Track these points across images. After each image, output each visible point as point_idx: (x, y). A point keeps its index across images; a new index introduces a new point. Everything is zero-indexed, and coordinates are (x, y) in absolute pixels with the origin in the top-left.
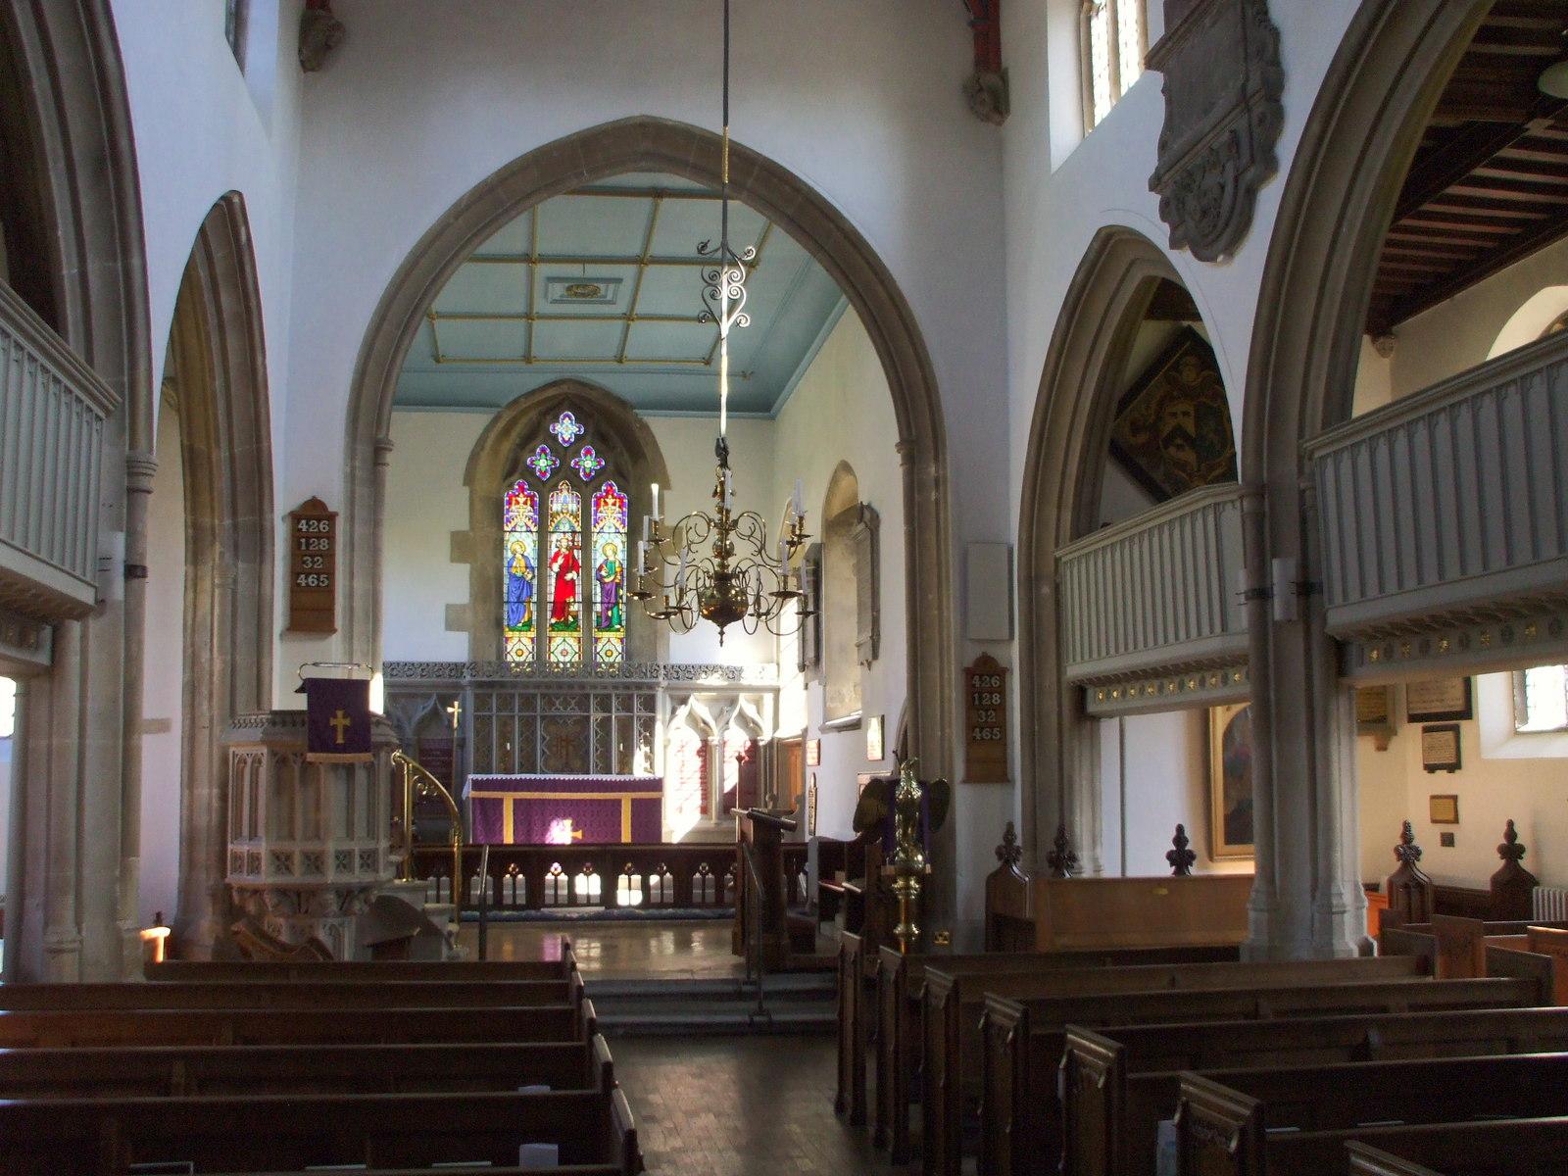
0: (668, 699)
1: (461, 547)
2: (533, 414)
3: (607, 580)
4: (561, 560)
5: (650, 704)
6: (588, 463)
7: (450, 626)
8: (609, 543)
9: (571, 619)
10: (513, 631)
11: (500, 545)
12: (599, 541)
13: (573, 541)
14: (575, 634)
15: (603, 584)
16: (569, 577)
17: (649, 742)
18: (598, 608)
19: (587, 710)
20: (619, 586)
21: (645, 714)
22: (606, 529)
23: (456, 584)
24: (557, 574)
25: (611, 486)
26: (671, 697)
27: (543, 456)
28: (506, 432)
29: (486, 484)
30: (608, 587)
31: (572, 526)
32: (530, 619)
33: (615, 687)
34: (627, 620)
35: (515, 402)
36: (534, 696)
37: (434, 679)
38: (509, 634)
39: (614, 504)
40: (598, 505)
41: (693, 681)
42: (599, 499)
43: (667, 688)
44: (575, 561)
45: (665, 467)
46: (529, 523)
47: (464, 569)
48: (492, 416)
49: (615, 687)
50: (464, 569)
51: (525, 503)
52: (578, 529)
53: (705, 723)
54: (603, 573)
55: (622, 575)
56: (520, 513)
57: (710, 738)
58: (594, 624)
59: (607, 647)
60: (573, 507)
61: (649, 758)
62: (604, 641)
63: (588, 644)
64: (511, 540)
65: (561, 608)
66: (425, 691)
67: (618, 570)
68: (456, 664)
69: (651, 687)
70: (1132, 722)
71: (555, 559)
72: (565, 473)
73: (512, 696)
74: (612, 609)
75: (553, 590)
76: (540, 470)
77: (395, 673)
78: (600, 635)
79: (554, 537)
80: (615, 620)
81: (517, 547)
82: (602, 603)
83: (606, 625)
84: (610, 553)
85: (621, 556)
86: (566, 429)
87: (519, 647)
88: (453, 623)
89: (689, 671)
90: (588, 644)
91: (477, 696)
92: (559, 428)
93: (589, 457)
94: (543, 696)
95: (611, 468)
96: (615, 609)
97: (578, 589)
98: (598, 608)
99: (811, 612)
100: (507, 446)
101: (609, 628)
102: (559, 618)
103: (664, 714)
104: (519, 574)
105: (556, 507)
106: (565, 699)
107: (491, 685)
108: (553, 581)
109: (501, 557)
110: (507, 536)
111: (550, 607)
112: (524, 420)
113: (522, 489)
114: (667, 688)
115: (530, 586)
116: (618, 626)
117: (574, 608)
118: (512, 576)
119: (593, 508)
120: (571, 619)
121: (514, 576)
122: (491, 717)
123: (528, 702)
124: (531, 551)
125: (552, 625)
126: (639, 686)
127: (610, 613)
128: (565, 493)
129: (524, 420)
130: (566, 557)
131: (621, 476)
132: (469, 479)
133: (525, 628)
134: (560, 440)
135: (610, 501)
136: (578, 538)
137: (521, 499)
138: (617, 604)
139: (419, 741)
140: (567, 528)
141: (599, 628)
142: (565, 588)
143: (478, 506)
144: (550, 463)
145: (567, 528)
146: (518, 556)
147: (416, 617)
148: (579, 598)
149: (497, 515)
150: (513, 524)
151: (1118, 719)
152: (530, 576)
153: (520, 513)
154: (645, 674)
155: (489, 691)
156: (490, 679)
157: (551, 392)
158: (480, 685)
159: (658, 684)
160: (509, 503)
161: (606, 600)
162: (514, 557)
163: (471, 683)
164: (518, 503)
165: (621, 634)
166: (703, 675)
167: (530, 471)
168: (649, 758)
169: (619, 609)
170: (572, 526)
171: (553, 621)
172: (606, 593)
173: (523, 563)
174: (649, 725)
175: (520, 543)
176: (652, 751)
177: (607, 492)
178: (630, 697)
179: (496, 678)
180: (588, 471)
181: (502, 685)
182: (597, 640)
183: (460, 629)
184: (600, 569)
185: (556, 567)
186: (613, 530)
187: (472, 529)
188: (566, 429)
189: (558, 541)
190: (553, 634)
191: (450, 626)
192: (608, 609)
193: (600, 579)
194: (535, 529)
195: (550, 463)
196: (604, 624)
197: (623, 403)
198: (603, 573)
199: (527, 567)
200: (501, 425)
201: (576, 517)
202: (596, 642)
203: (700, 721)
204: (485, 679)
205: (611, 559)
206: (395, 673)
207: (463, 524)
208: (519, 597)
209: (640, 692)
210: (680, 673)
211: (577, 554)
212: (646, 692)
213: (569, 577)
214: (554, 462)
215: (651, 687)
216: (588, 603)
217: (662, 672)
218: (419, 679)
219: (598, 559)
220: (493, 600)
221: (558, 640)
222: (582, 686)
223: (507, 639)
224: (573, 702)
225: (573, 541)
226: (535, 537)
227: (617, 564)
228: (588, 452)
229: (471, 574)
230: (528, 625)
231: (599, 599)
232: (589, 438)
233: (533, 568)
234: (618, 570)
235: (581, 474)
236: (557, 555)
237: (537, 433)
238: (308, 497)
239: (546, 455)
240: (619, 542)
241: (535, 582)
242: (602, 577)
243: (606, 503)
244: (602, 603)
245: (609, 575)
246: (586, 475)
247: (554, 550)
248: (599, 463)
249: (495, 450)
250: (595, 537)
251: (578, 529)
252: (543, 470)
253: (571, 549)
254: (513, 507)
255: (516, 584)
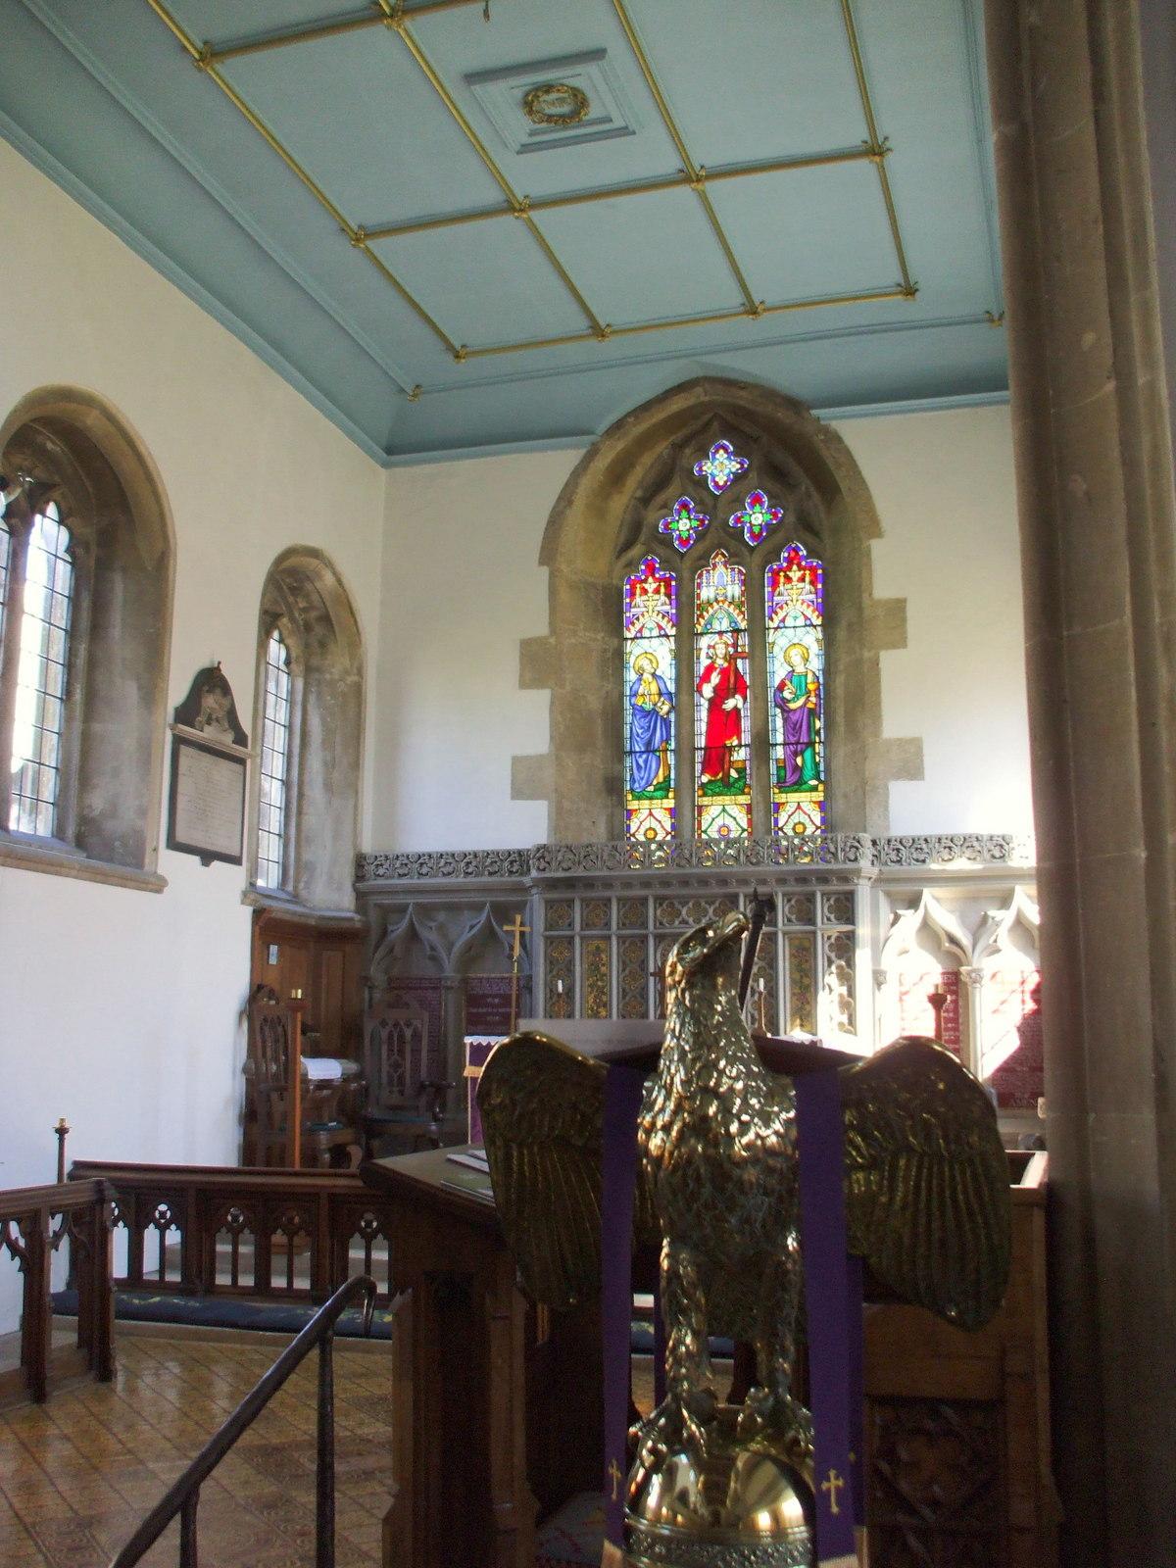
0: (882, 897)
1: (537, 663)
2: (662, 448)
3: (792, 706)
4: (715, 678)
5: (845, 908)
6: (757, 517)
7: (518, 792)
8: (796, 646)
9: (734, 774)
10: (639, 799)
11: (616, 660)
12: (779, 640)
13: (735, 645)
14: (744, 799)
15: (786, 711)
16: (729, 704)
17: (847, 978)
18: (779, 752)
19: (812, 921)
20: (812, 713)
21: (837, 929)
22: (789, 622)
23: (527, 723)
24: (711, 701)
25: (796, 550)
26: (888, 894)
27: (684, 514)
28: (616, 476)
29: (586, 559)
30: (794, 718)
31: (733, 621)
32: (667, 778)
33: (782, 881)
34: (827, 770)
35: (618, 426)
36: (644, 901)
37: (486, 879)
38: (633, 805)
39: (802, 579)
40: (775, 584)
41: (924, 867)
42: (775, 574)
43: (880, 881)
44: (739, 677)
45: (869, 497)
46: (664, 623)
47: (542, 697)
48: (583, 452)
49: (782, 881)
50: (542, 697)
51: (657, 591)
52: (743, 625)
53: (953, 940)
54: (787, 694)
55: (818, 696)
56: (650, 608)
57: (963, 969)
58: (774, 780)
59: (795, 819)
60: (735, 590)
61: (848, 1005)
62: (790, 808)
63: (764, 813)
64: (634, 651)
65: (716, 758)
66: (476, 898)
67: (811, 687)
68: (520, 853)
69: (844, 877)
70: (51, 1180)
71: (706, 678)
72: (721, 539)
73: (607, 902)
74: (802, 753)
75: (704, 728)
76: (680, 537)
77: (424, 870)
78: (781, 798)
79: (704, 642)
80: (808, 772)
81: (645, 663)
82: (785, 744)
83: (793, 780)
84: (797, 660)
85: (816, 664)
86: (720, 467)
87: (650, 819)
88: (522, 788)
89: (919, 847)
90: (764, 813)
91: (550, 904)
92: (708, 467)
93: (757, 508)
94: (660, 900)
95: (791, 519)
96: (808, 754)
97: (746, 724)
98: (779, 752)
99: (592, 454)
100: (620, 504)
101: (798, 785)
102: (714, 774)
103: (875, 922)
104: (648, 707)
105: (706, 593)
106: (697, 905)
107: (570, 883)
108: (703, 714)
109: (620, 681)
110: (629, 646)
111: (699, 756)
112: (647, 460)
113: (651, 570)
114: (880, 881)
115: (666, 722)
116: (814, 782)
117: (740, 755)
118: (638, 711)
119: (767, 589)
120: (734, 774)
121: (642, 709)
122: (572, 937)
123: (634, 909)
124: (667, 670)
125: (703, 786)
126: (823, 878)
127: (799, 760)
128: (721, 568)
129: (647, 460)
130: (724, 672)
131: (807, 527)
132: (549, 553)
133: (659, 794)
134: (711, 485)
135: (795, 574)
136: (744, 640)
137: (651, 585)
138: (811, 744)
139: (465, 981)
140: (725, 625)
141: (783, 786)
142: (724, 724)
143: (564, 595)
144: (695, 524)
145: (725, 625)
146: (647, 677)
147: (468, 782)
148: (746, 738)
149: (612, 613)
150: (638, 626)
151: (487, 1170)
152: (666, 708)
153: (650, 608)
154: (835, 855)
155: (568, 895)
156: (567, 874)
157: (677, 405)
158: (552, 884)
159: (858, 872)
160: (632, 595)
161: (793, 740)
162: (640, 679)
163: (537, 882)
164: (645, 591)
165: (819, 796)
166: (945, 855)
167: (665, 540)
168: (848, 1005)
169: (814, 753)
170: (733, 621)
171: (705, 779)
172: (792, 727)
173: (654, 688)
174: (845, 947)
175: (650, 657)
176: (851, 993)
177: (790, 561)
178: (810, 898)
179: (579, 872)
180: (756, 530)
181: (589, 883)
182: (778, 806)
183: (534, 796)
184: (782, 687)
185: (708, 690)
186: (801, 621)
187: (553, 631)
188: (720, 467)
189: (712, 648)
190: (706, 801)
191: (518, 792)
192: (796, 754)
193: (782, 704)
194: (672, 631)
195: (695, 524)
196: (790, 779)
197: (794, 405)
198: (787, 694)
199: (660, 694)
200: (602, 463)
201: (739, 606)
202: (777, 810)
203: (944, 938)
204: (561, 874)
205: (800, 669)
206: (424, 870)
207: (541, 629)
208: (649, 743)
209: (788, 889)
210: (903, 851)
211: (742, 665)
212: (836, 886)
213: (729, 704)
214: (702, 521)
215: (844, 877)
216: (762, 744)
217: (868, 851)
218: (461, 879)
219: (778, 671)
220: (599, 741)
221: (714, 810)
222: (723, 881)
223: (630, 813)
224: (711, 911)
225: (735, 645)
226: (672, 644)
227: (810, 678)
228: (757, 500)
229: (552, 703)
230: (664, 788)
231: (780, 738)
232: (753, 475)
233: (670, 693)
234: (811, 687)
235: (747, 536)
236: (710, 669)
237: (672, 477)
238: (927, 772)
239: (689, 512)
240: (812, 639)
241: (672, 717)
242: (785, 701)
243: (789, 579)
244: (785, 744)
245: (796, 698)
246: (754, 536)
247: (705, 662)
248: (775, 515)
249: (598, 510)
250: (771, 637)
251: (743, 625)
252: (685, 535)
253: (731, 659)
254: (638, 599)
255: (644, 722)
